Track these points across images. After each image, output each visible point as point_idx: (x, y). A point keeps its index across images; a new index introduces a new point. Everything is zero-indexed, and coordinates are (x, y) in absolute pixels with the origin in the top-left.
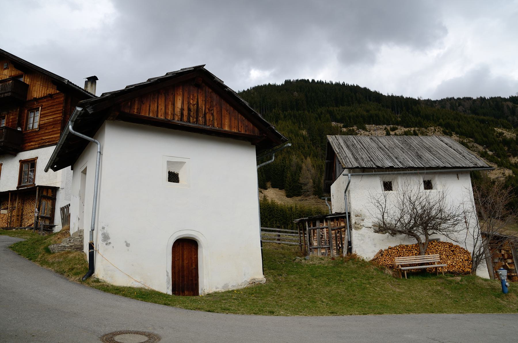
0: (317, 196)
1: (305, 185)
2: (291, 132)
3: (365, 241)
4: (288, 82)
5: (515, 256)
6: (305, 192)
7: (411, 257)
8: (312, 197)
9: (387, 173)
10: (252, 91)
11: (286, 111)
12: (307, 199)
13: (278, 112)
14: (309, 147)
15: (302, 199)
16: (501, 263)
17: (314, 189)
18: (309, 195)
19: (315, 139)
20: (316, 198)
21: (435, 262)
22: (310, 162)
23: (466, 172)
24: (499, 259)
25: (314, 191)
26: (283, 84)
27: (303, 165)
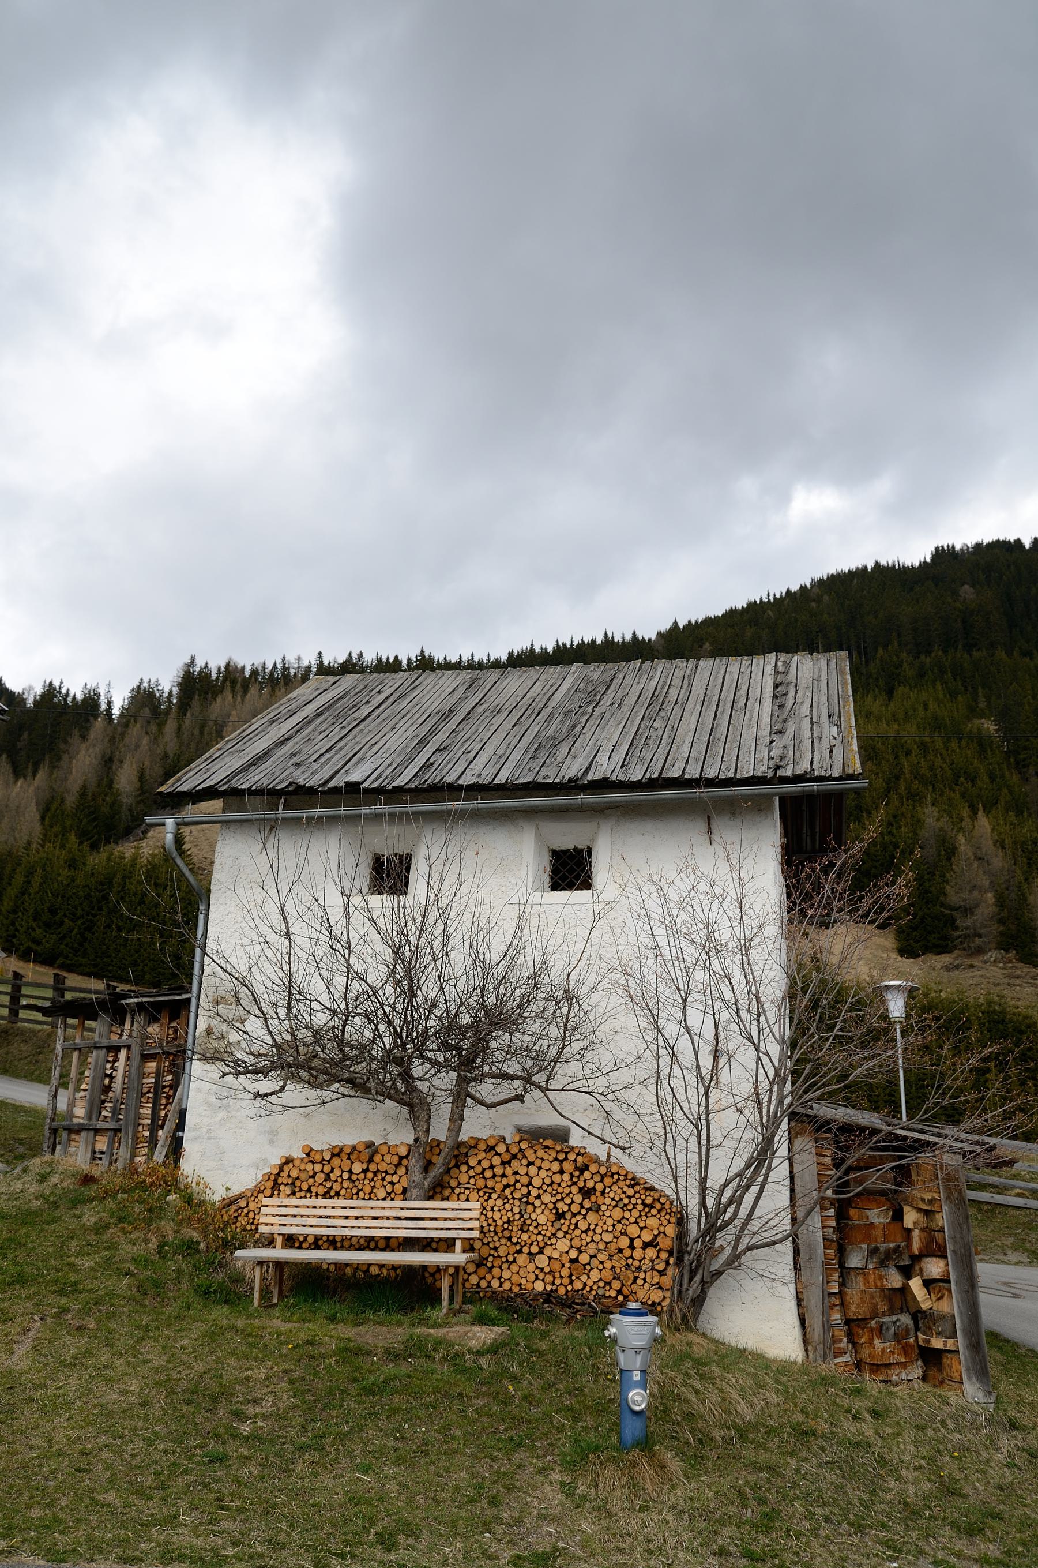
0: (1012, 954)
1: (967, 911)
2: (936, 724)
3: (234, 1113)
4: (944, 556)
5: (955, 1242)
6: (966, 936)
7: (380, 1203)
8: (993, 955)
9: (342, 811)
10: (816, 590)
11: (928, 652)
12: (976, 963)
13: (895, 658)
14: (992, 778)
15: (957, 962)
16: (881, 1277)
17: (1002, 928)
18: (980, 951)
19: (1026, 748)
20: (1010, 962)
21: (454, 1239)
22: (989, 830)
23: (759, 806)
24: (873, 1252)
25: (1001, 934)
26: (925, 562)
27: (961, 839)
